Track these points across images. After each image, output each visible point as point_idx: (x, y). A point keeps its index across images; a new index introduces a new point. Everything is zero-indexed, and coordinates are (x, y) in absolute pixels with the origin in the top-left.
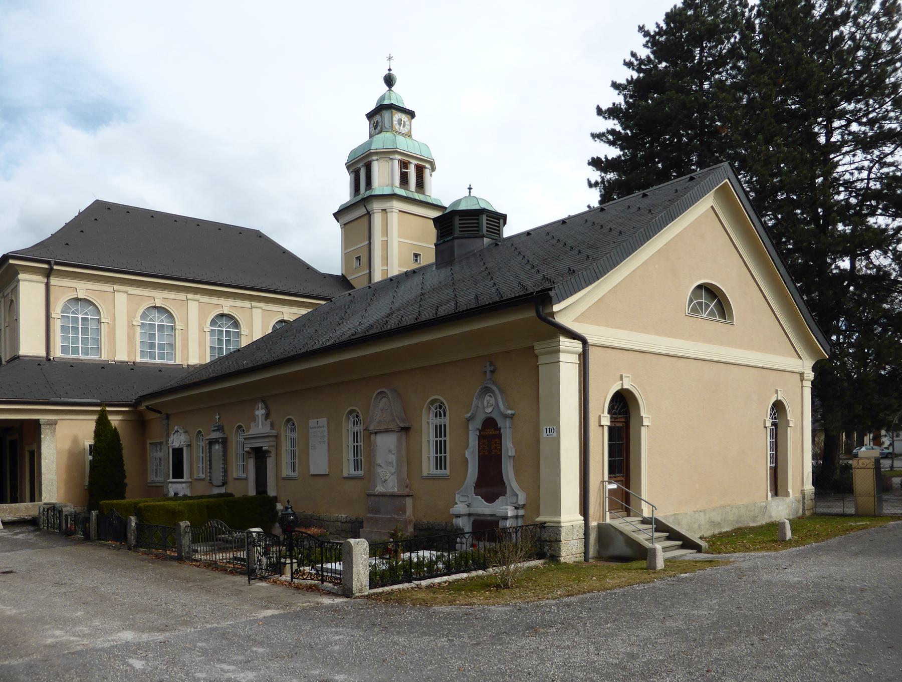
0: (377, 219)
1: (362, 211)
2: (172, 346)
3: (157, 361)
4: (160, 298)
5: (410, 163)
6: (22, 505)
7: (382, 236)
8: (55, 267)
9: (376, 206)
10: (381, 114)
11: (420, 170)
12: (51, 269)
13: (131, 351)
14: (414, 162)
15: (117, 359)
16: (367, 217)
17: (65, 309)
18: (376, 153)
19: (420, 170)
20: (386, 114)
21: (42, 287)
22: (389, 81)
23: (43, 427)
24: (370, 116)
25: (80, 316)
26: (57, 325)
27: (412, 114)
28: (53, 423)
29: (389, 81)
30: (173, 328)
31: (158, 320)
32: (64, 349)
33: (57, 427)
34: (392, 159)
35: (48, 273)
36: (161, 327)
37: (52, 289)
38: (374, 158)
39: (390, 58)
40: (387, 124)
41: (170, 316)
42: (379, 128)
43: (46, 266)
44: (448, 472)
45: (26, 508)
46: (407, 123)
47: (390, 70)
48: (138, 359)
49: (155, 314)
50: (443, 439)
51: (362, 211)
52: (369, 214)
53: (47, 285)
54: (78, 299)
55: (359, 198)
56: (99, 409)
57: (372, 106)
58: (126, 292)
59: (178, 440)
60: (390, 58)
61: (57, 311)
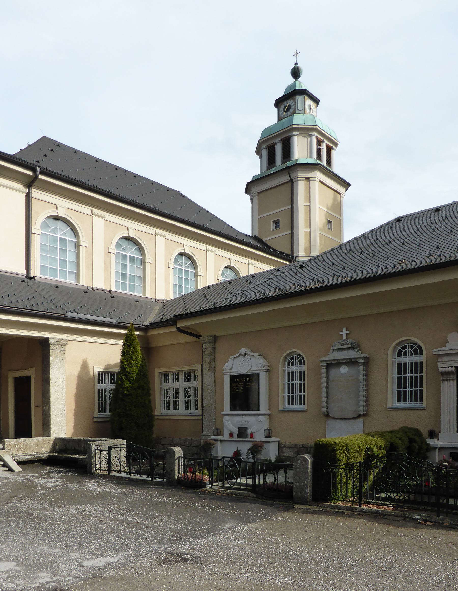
0: (301, 186)
1: (286, 178)
2: (143, 279)
3: (128, 292)
4: (135, 229)
5: (323, 141)
6: (32, 440)
7: (305, 202)
8: (41, 177)
9: (301, 175)
10: (287, 102)
11: (329, 149)
12: (36, 177)
13: (107, 279)
14: (326, 141)
15: (94, 286)
16: (289, 185)
17: (45, 225)
18: (297, 129)
19: (329, 149)
20: (299, 99)
21: (23, 197)
22: (296, 73)
23: (52, 347)
24: (278, 103)
25: (59, 236)
26: (36, 242)
27: (316, 101)
28: (62, 344)
29: (296, 73)
30: (143, 262)
31: (131, 252)
32: (43, 268)
33: (67, 347)
34: (311, 136)
35: (30, 183)
36: (132, 259)
37: (34, 203)
38: (295, 133)
39: (296, 54)
40: (300, 107)
41: (141, 249)
42: (291, 111)
43: (30, 173)
44: (424, 404)
45: (37, 444)
46: (315, 110)
47: (296, 64)
48: (113, 289)
49: (127, 244)
50: (419, 375)
51: (286, 178)
52: (292, 183)
53: (28, 196)
54: (56, 218)
55: (273, 171)
56: (124, 332)
57: (281, 94)
58: (103, 217)
59: (240, 366)
60: (296, 54)
61: (36, 228)
